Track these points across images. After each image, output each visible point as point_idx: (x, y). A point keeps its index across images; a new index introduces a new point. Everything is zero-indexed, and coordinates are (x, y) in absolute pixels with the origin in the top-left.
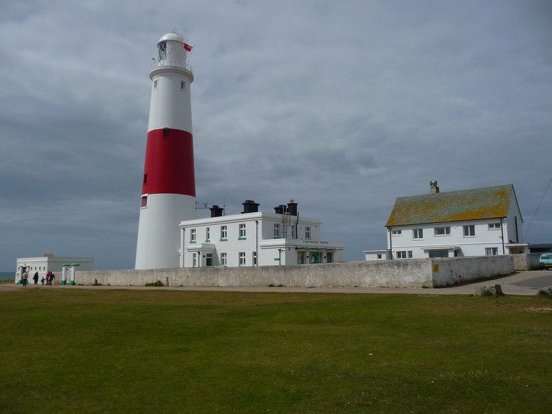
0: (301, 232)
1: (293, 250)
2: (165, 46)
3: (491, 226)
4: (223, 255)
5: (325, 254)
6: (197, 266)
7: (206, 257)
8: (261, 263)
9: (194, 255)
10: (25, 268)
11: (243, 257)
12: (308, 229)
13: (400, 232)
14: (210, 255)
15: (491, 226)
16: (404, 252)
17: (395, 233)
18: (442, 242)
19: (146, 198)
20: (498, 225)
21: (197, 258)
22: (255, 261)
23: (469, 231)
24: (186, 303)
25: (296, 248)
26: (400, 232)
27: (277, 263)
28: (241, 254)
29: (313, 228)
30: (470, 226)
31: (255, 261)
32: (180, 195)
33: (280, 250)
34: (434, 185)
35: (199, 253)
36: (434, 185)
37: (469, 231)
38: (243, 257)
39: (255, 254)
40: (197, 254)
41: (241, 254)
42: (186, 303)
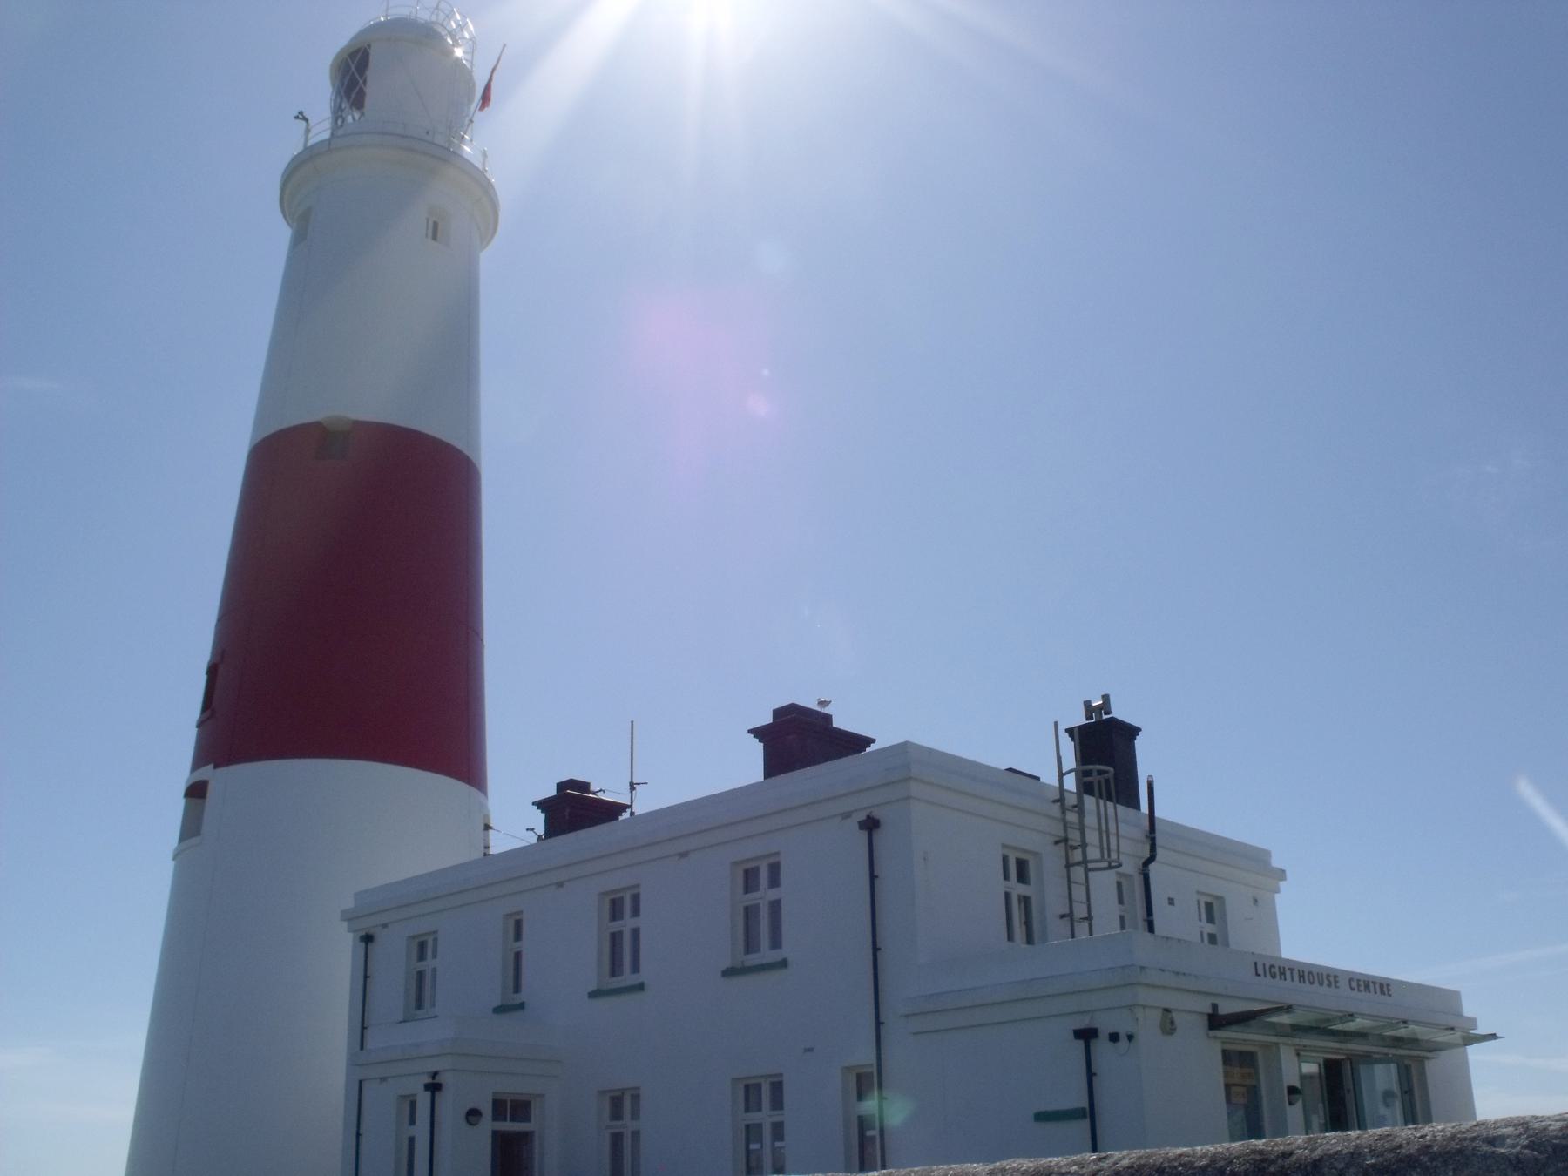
0: (1178, 919)
7: (487, 1125)
11: (765, 1117)
25: (1216, 1021)
28: (750, 1093)
33: (1086, 1035)
40: (424, 1099)
41: (750, 1093)
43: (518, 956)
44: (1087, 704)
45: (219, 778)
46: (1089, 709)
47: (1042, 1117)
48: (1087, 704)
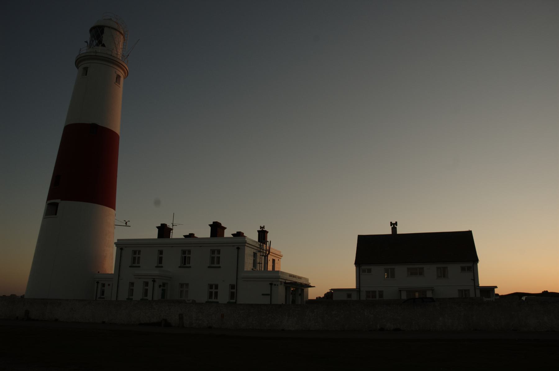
2: (102, 32)
3: (463, 269)
4: (182, 285)
6: (149, 297)
8: (243, 298)
9: (146, 284)
11: (214, 290)
12: (274, 260)
13: (369, 271)
14: (164, 285)
15: (463, 269)
17: (364, 271)
21: (150, 288)
22: (146, 293)
23: (443, 274)
24: (121, 46)
25: (285, 283)
26: (369, 271)
27: (266, 301)
28: (211, 286)
31: (233, 295)
32: (53, 169)
33: (271, 284)
34: (394, 226)
36: (394, 226)
37: (443, 274)
38: (214, 290)
39: (232, 287)
41: (211, 286)
42: (121, 46)
44: (391, 223)
45: (63, 205)
46: (261, 227)
47: (263, 295)
48: (391, 223)
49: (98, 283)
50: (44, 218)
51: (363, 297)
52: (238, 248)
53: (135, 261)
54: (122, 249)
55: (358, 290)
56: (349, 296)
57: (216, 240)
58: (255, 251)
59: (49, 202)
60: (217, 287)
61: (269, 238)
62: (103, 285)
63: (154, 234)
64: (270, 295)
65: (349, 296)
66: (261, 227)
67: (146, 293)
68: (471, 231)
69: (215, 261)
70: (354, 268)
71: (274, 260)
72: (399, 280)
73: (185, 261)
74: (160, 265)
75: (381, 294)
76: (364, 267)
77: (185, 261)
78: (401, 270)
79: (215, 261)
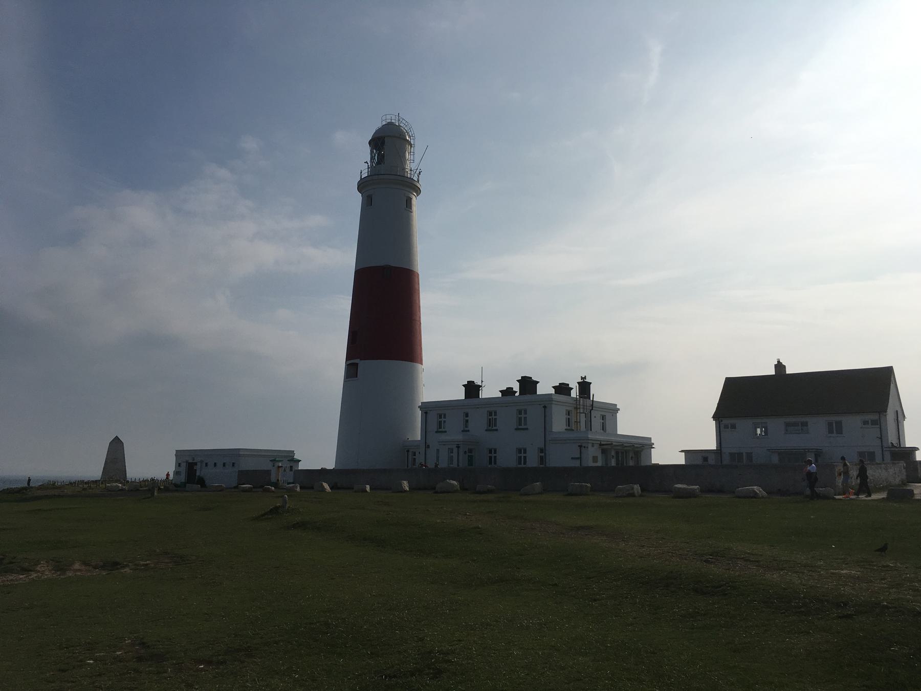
0: (596, 423)
1: (596, 446)
2: (383, 143)
3: (865, 423)
5: (631, 454)
9: (451, 450)
10: (196, 464)
11: (522, 455)
12: (603, 417)
14: (470, 451)
16: (740, 455)
17: (726, 427)
18: (795, 441)
19: (357, 364)
20: (874, 422)
25: (601, 445)
26: (734, 427)
27: (576, 464)
29: (608, 416)
30: (836, 423)
31: (542, 460)
33: (580, 446)
35: (458, 447)
37: (836, 429)
38: (522, 455)
39: (542, 451)
40: (455, 450)
41: (519, 451)
43: (467, 421)
45: (363, 365)
46: (582, 378)
49: (408, 451)
50: (345, 381)
51: (726, 460)
52: (545, 407)
53: (440, 429)
54: (426, 413)
55: (718, 452)
56: (706, 459)
57: (528, 397)
58: (569, 409)
59: (349, 362)
60: (525, 452)
61: (593, 390)
62: (414, 454)
63: (460, 395)
64: (580, 458)
65: (706, 459)
66: (582, 378)
67: (451, 459)
68: (892, 367)
69: (521, 424)
70: (713, 424)
71: (603, 417)
72: (766, 435)
73: (491, 425)
74: (888, 456)
75: (749, 455)
76: (726, 421)
77: (491, 425)
78: (777, 425)
79: (521, 424)
